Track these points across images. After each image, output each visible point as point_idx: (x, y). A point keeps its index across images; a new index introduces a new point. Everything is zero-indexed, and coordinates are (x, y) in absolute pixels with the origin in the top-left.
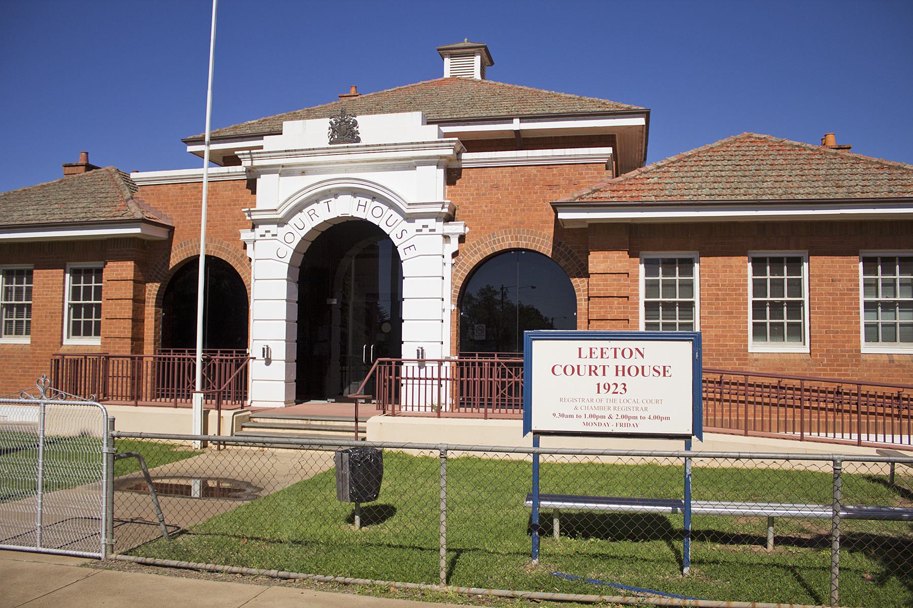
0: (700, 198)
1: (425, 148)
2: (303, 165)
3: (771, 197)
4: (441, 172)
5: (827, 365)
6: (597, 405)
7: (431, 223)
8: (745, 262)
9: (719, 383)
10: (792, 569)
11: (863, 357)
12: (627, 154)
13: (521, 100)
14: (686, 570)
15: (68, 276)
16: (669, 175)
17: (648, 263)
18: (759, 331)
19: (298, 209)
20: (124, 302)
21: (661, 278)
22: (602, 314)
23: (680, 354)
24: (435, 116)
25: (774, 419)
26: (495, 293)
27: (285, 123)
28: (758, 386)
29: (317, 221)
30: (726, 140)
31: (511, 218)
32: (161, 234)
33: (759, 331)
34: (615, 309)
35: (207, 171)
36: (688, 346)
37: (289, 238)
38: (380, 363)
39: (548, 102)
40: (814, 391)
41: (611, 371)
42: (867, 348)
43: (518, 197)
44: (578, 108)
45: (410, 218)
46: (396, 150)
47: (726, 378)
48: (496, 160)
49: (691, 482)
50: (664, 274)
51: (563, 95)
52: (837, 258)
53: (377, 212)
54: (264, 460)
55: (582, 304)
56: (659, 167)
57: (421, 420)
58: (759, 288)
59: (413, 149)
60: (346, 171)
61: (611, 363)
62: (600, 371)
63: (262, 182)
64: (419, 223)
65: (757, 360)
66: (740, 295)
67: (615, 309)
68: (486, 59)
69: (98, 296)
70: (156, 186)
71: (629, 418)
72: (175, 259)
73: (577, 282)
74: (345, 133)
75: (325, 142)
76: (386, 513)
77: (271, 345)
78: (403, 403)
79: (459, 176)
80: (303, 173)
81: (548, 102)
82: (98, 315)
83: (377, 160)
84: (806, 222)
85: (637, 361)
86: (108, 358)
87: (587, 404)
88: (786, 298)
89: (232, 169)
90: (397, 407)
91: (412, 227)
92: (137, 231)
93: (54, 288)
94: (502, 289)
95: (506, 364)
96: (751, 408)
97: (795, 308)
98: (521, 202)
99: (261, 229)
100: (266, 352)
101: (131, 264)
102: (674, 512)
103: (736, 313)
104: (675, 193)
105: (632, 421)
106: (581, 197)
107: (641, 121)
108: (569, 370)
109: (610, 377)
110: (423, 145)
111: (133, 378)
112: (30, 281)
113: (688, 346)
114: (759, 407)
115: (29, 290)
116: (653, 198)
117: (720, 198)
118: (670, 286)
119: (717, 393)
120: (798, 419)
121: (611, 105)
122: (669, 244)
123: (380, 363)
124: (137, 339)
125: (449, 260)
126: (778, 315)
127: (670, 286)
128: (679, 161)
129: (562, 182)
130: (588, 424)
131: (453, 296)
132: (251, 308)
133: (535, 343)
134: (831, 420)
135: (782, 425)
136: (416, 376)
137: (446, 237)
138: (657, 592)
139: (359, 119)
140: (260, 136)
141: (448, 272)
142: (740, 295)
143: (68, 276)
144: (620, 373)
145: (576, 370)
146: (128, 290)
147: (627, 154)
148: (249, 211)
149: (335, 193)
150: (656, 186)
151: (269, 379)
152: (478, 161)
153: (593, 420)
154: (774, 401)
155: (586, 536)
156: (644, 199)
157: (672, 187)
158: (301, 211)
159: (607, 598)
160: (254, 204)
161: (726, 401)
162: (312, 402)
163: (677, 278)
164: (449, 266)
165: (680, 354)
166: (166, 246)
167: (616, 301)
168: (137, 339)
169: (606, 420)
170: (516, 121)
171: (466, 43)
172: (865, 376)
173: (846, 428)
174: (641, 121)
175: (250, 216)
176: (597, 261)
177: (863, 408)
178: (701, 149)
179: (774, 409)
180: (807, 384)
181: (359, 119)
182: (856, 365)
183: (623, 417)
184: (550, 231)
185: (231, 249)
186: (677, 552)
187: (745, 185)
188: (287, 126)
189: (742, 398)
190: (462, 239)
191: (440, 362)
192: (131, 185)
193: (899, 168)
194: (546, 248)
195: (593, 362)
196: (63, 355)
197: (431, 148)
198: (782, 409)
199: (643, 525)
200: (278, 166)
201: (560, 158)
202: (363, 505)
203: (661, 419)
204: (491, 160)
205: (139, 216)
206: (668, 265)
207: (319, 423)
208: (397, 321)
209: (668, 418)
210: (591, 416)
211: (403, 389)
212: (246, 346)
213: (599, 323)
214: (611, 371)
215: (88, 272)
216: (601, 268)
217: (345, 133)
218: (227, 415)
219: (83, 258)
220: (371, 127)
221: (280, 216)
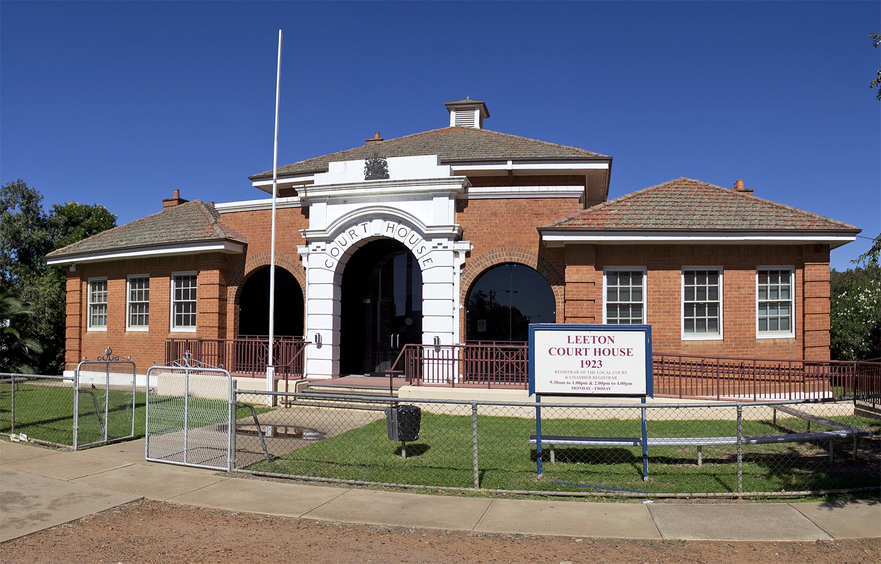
0: (648, 226)
1: (440, 184)
2: (345, 195)
3: (698, 227)
4: (453, 202)
5: (735, 348)
6: (581, 375)
7: (445, 241)
8: (679, 274)
9: (661, 362)
10: (714, 475)
11: (757, 342)
12: (596, 191)
13: (512, 146)
14: (646, 478)
15: (172, 281)
16: (626, 208)
17: (609, 274)
18: (689, 325)
19: (342, 230)
20: (212, 300)
21: (618, 286)
22: (575, 313)
23: (636, 340)
24: (446, 158)
25: (700, 387)
26: (485, 296)
27: (330, 164)
28: (689, 364)
29: (356, 239)
30: (667, 183)
31: (506, 239)
32: (238, 249)
33: (689, 325)
34: (584, 309)
35: (274, 201)
36: (642, 335)
37: (335, 252)
38: (408, 347)
39: (534, 148)
40: (726, 366)
41: (591, 352)
42: (760, 335)
43: (511, 223)
44: (557, 154)
45: (428, 238)
46: (418, 185)
47: (666, 359)
48: (495, 193)
49: (645, 428)
50: (621, 284)
51: (545, 143)
52: (742, 272)
53: (403, 233)
54: (320, 415)
55: (560, 306)
56: (618, 202)
57: (440, 388)
58: (689, 293)
59: (431, 184)
60: (378, 201)
61: (591, 346)
62: (583, 352)
63: (314, 209)
64: (435, 242)
65: (687, 346)
66: (676, 298)
67: (584, 309)
68: (484, 113)
69: (194, 297)
70: (234, 213)
71: (604, 384)
72: (249, 268)
73: (556, 289)
74: (377, 172)
75: (361, 178)
76: (421, 449)
77: (322, 333)
78: (426, 377)
79: (466, 205)
80: (345, 202)
81: (534, 148)
82: (194, 310)
83: (402, 192)
84: (722, 246)
85: (609, 345)
86: (201, 341)
87: (574, 375)
88: (707, 301)
89: (290, 199)
90: (421, 380)
91: (429, 245)
92: (222, 247)
93: (163, 290)
94: (491, 293)
95: (503, 349)
96: (683, 380)
97: (714, 308)
98: (514, 226)
99: (314, 245)
100: (318, 338)
101: (217, 272)
102: (635, 445)
103: (672, 312)
104: (630, 222)
105: (606, 386)
106: (560, 224)
107: (605, 166)
108: (561, 352)
109: (591, 357)
110: (438, 181)
111: (219, 357)
112: (147, 286)
113: (642, 335)
114: (689, 379)
115: (147, 293)
116: (614, 226)
117: (663, 227)
118: (625, 292)
119: (662, 369)
120: (715, 386)
121: (583, 153)
122: (624, 261)
123: (408, 347)
124: (222, 328)
125: (458, 271)
126: (701, 314)
127: (625, 292)
128: (633, 197)
129: (546, 212)
130: (575, 388)
131: (461, 298)
132: (306, 305)
133: (536, 333)
134: (737, 386)
135: (705, 391)
136: (431, 357)
137: (456, 253)
138: (628, 490)
139: (388, 160)
140: (312, 173)
141: (457, 279)
142: (676, 298)
143: (172, 281)
144: (597, 354)
145: (566, 351)
146: (215, 292)
147: (596, 191)
148: (305, 231)
149: (370, 218)
150: (616, 217)
151: (320, 360)
152: (481, 194)
153: (579, 385)
154: (699, 374)
155: (574, 461)
156: (607, 226)
157: (629, 217)
158: (344, 231)
159: (594, 494)
160: (308, 226)
161: (666, 375)
162: (351, 376)
163: (631, 286)
164: (458, 275)
165: (636, 340)
166: (241, 259)
167: (585, 303)
168: (222, 328)
169: (588, 386)
170: (510, 163)
171: (468, 100)
172: (759, 354)
173: (747, 391)
174: (605, 166)
175: (305, 235)
176: (572, 273)
177: (757, 377)
178: (650, 188)
179: (699, 380)
180: (721, 362)
181: (388, 160)
182: (753, 347)
183: (600, 383)
184: (536, 249)
185: (290, 260)
186: (639, 469)
187: (681, 217)
188: (332, 165)
189: (677, 373)
190: (468, 254)
191: (453, 347)
192: (215, 213)
193: (783, 208)
194: (533, 262)
195: (578, 346)
196: (173, 339)
197: (444, 184)
198: (704, 380)
199: (612, 455)
200: (326, 196)
201: (544, 193)
202: (407, 443)
203: (627, 384)
204: (491, 193)
205: (222, 236)
206: (625, 276)
207: (360, 390)
208: (417, 317)
209: (631, 384)
210: (577, 383)
211: (426, 366)
212: (302, 333)
213: (572, 320)
214: (591, 352)
215: (186, 278)
216: (575, 278)
217: (377, 172)
218: (292, 383)
219: (181, 269)
220: (400, 167)
221: (328, 235)
